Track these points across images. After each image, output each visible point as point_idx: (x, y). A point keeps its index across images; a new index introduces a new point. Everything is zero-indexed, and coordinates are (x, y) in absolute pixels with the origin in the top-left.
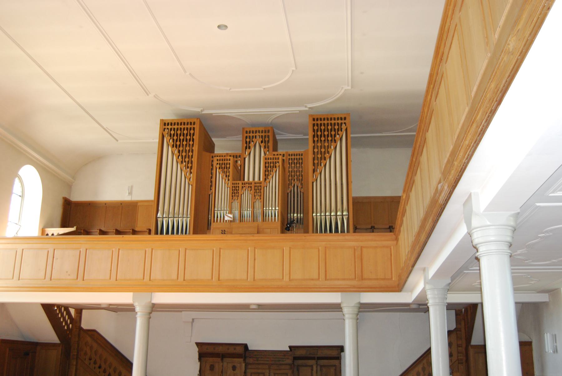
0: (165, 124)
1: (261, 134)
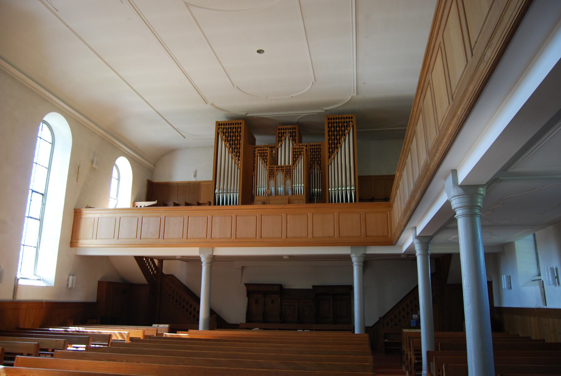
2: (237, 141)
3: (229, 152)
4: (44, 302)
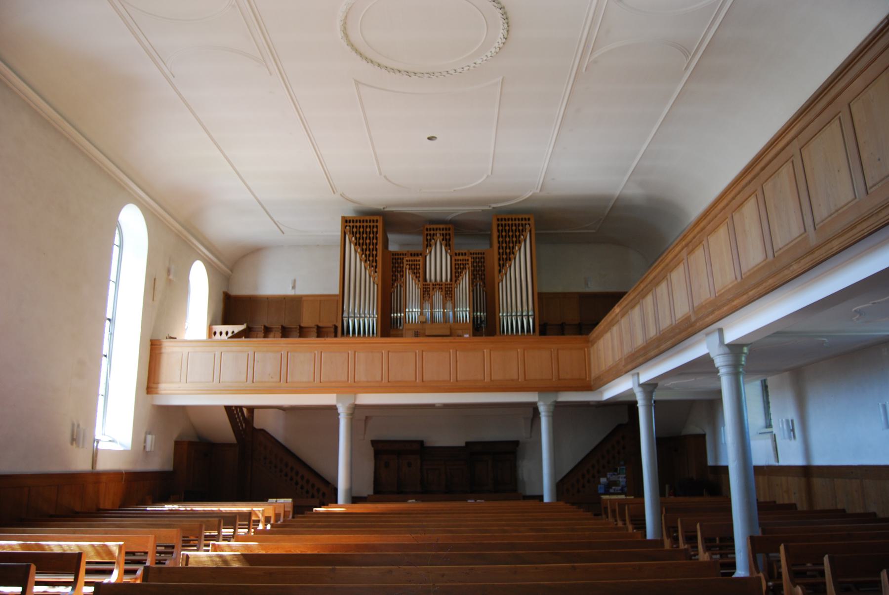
0: (346, 221)
1: (441, 232)
2: (373, 245)
3: (361, 260)
4: (124, 472)
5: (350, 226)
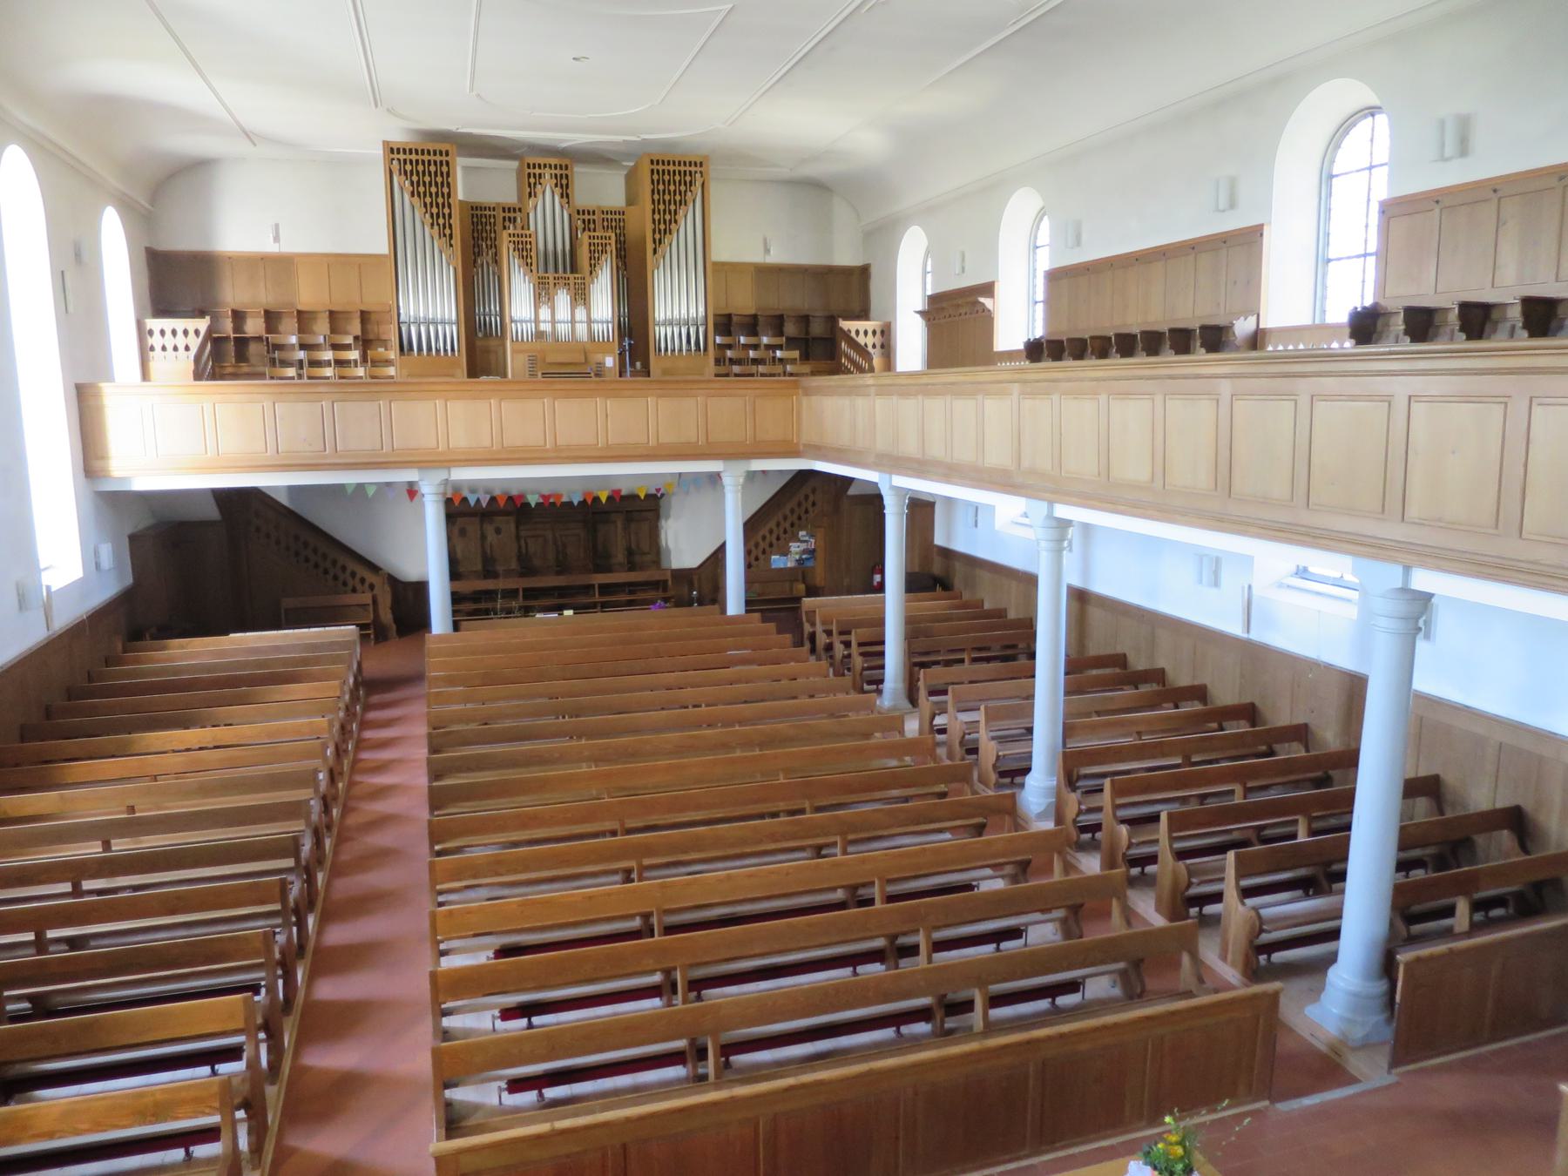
5: (399, 160)
